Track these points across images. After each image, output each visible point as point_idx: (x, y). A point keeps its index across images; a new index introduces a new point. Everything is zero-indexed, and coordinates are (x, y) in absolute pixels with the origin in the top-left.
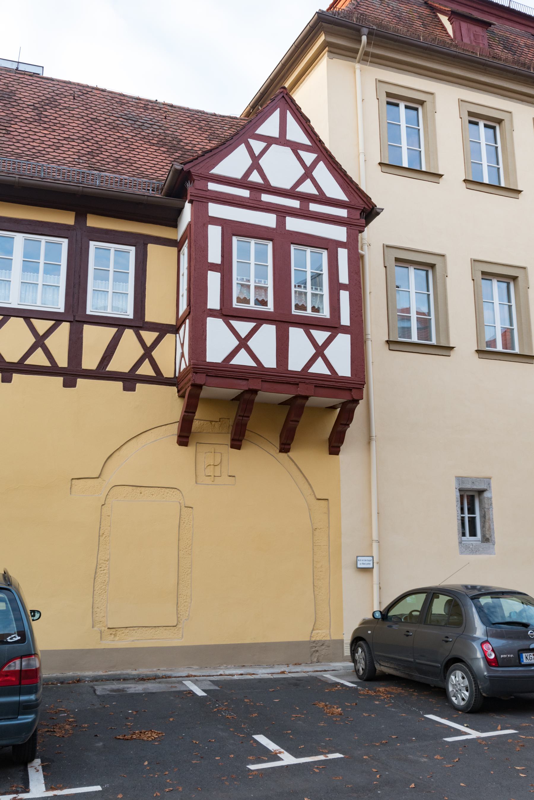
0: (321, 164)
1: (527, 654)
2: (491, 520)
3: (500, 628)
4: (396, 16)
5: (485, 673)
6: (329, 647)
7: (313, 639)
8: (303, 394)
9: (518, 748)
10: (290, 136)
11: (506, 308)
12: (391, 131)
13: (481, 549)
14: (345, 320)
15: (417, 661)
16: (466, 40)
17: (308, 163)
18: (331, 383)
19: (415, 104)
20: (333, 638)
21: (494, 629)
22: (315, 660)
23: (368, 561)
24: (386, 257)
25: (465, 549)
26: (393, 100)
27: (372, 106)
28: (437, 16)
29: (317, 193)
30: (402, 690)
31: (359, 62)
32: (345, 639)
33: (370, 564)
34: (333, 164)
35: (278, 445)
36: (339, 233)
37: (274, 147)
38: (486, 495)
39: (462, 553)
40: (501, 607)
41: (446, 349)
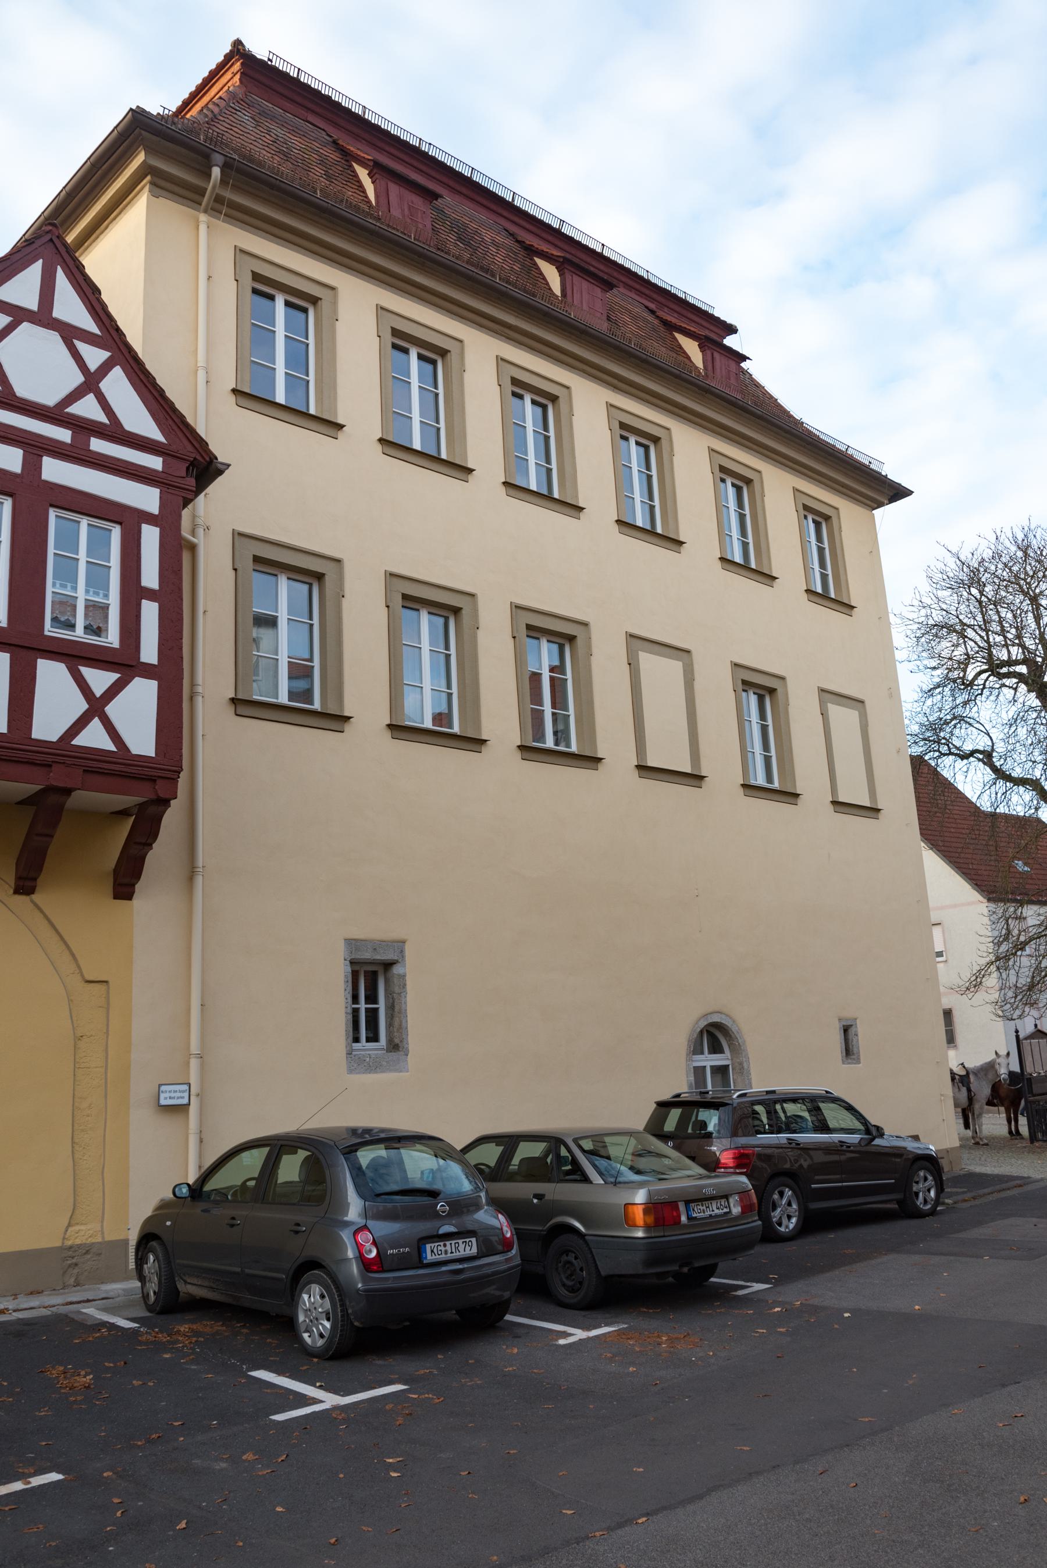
0: (117, 372)
1: (433, 1245)
2: (403, 1013)
3: (392, 1201)
4: (280, 152)
5: (360, 1285)
6: (100, 1254)
7: (69, 1243)
8: (61, 785)
9: (400, 1420)
10: (59, 312)
11: (442, 658)
12: (259, 336)
13: (384, 1063)
14: (149, 652)
15: (247, 1271)
16: (396, 212)
17: (93, 366)
18: (116, 767)
19: (302, 302)
20: (107, 1238)
21: (381, 1205)
22: (72, 1281)
23: (180, 1092)
24: (237, 553)
25: (356, 1064)
26: (264, 286)
27: (228, 293)
28: (351, 166)
29: (106, 421)
30: (222, 1326)
31: (205, 211)
32: (130, 1238)
33: (183, 1098)
34: (139, 373)
35: (12, 882)
36: (146, 498)
37: (26, 328)
38: (397, 970)
39: (350, 1071)
40: (401, 1163)
41: (336, 720)
